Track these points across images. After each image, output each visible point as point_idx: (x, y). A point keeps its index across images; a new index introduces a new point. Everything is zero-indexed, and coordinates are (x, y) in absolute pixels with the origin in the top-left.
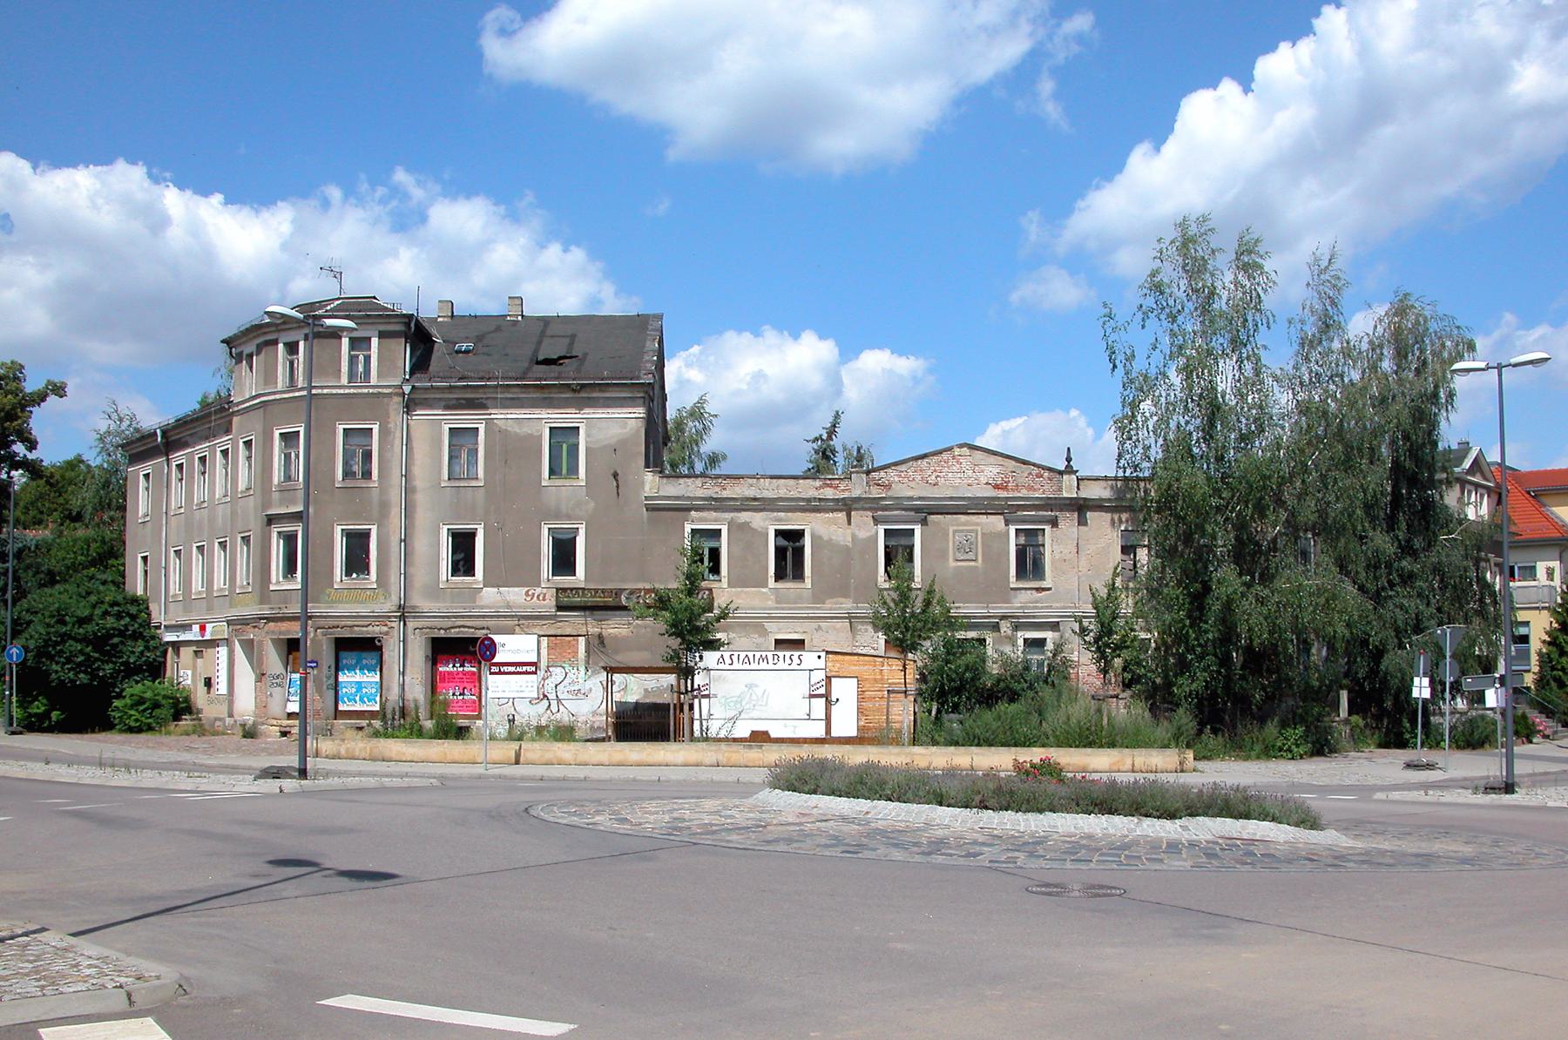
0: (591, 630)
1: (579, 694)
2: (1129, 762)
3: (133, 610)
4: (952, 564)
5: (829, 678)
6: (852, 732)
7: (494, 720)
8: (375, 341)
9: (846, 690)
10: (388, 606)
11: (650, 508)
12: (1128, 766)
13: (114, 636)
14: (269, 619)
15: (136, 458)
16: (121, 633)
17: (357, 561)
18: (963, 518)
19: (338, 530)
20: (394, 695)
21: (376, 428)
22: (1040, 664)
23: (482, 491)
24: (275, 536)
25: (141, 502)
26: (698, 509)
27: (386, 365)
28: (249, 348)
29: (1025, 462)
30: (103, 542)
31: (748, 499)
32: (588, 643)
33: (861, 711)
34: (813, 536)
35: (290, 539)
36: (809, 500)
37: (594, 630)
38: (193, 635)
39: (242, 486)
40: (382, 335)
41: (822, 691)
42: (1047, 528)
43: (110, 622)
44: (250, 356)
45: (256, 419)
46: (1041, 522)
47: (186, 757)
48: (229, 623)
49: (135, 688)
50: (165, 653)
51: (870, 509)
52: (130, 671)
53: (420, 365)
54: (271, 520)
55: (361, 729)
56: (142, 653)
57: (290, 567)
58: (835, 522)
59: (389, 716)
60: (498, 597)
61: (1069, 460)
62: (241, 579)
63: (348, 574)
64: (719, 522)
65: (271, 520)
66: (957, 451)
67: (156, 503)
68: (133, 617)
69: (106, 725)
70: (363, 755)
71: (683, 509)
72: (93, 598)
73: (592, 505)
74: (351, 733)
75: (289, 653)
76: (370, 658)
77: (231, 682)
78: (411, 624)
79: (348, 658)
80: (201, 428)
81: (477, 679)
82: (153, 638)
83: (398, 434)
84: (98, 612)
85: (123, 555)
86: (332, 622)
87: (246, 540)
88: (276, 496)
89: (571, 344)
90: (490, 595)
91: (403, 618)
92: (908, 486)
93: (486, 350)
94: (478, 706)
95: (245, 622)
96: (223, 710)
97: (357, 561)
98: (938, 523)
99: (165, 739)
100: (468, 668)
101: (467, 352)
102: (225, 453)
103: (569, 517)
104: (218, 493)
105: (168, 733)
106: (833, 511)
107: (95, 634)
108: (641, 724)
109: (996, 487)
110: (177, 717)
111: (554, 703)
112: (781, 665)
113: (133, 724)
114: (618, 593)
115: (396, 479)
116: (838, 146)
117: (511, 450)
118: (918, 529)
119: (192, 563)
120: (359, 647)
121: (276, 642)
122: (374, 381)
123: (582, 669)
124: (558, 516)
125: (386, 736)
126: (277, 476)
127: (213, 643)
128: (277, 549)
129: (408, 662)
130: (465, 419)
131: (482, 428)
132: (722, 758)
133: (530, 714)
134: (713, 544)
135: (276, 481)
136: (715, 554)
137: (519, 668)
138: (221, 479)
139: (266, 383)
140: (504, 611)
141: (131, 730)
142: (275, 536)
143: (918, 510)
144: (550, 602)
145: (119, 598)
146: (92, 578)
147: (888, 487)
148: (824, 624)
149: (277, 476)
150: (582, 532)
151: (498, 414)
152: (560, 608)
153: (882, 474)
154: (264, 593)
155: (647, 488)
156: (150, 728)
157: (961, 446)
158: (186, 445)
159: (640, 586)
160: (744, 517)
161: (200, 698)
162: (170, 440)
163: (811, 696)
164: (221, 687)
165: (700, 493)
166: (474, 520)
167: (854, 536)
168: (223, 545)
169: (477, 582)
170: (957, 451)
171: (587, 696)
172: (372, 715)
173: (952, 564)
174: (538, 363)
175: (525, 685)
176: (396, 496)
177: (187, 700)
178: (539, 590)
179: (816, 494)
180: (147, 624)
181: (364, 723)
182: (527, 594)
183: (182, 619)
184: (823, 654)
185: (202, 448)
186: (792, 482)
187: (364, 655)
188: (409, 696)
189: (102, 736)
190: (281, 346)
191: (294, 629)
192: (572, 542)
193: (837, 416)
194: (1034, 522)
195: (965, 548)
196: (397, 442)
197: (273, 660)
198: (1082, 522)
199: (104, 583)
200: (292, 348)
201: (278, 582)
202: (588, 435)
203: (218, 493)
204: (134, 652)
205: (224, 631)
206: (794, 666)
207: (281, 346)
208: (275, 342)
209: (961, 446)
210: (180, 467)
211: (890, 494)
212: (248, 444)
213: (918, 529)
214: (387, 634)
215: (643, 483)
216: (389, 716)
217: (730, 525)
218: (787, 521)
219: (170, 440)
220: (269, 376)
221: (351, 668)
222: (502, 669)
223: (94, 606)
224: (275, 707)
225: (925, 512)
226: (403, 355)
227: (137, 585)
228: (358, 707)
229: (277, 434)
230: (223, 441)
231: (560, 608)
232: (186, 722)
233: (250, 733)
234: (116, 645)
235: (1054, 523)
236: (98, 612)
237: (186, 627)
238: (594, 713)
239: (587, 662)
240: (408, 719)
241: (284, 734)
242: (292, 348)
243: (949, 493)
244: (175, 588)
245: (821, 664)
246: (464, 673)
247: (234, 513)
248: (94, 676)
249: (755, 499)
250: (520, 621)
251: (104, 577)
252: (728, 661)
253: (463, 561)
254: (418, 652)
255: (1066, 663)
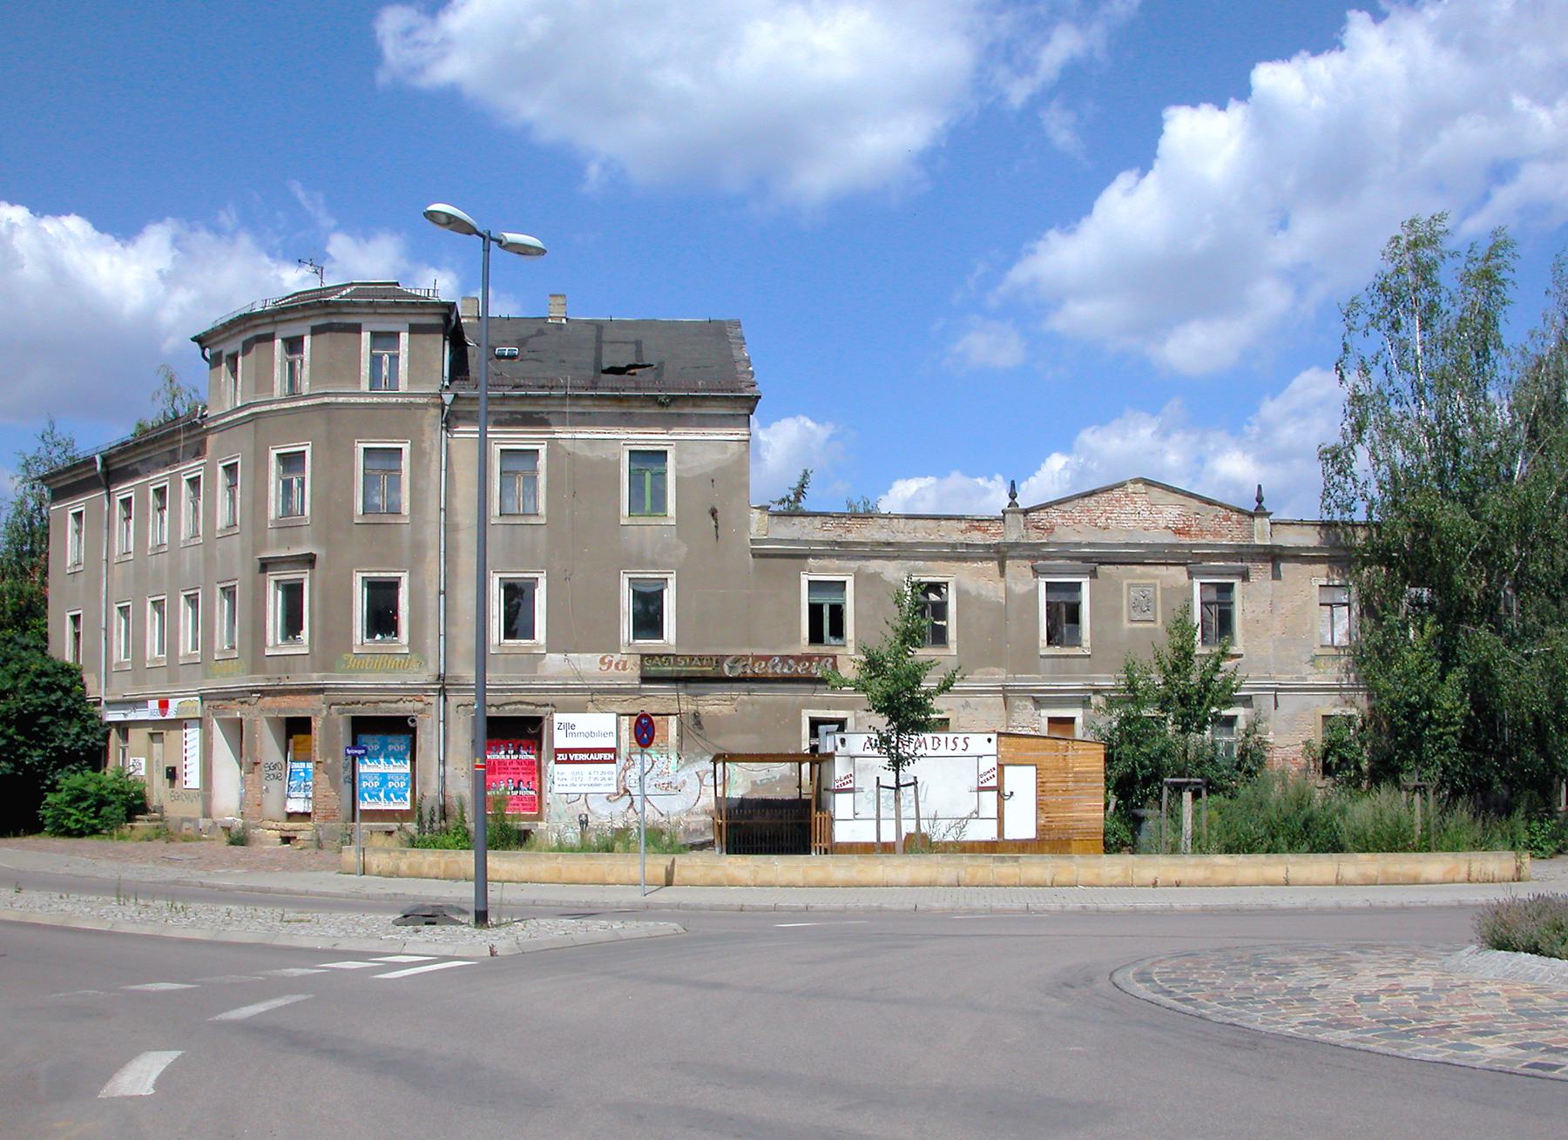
0: (684, 708)
1: (670, 788)
2: (1464, 869)
3: (66, 682)
4: (1126, 625)
5: (1001, 767)
6: (1029, 833)
7: (556, 823)
8: (404, 337)
9: (1021, 780)
10: (423, 676)
11: (757, 555)
12: (1463, 875)
13: (43, 714)
14: (264, 693)
15: (60, 494)
16: (52, 710)
17: (382, 619)
18: (1139, 569)
19: (358, 580)
20: (431, 791)
21: (406, 448)
22: (1229, 747)
23: (543, 531)
24: (271, 586)
25: (69, 548)
26: (816, 556)
27: (416, 366)
28: (235, 345)
29: (1210, 502)
30: (20, 596)
31: (879, 544)
32: (681, 723)
33: (1041, 806)
34: (959, 592)
35: (293, 593)
36: (954, 546)
37: (688, 706)
38: (151, 712)
39: (222, 520)
40: (414, 330)
41: (993, 783)
42: (1237, 582)
43: (36, 699)
44: (233, 358)
45: (244, 436)
46: (1230, 575)
47: (171, 873)
48: (203, 698)
49: (72, 780)
50: (107, 736)
51: (1028, 557)
52: (65, 759)
53: (459, 368)
54: (265, 565)
55: (390, 833)
56: (78, 735)
57: (292, 624)
58: (983, 573)
59: (427, 817)
60: (565, 666)
61: (1260, 500)
62: (221, 642)
63: (371, 635)
64: (842, 572)
65: (265, 565)
66: (1130, 488)
67: (93, 549)
68: (67, 691)
69: (34, 827)
70: (434, 872)
71: (797, 556)
72: (14, 667)
73: (684, 550)
74: (379, 840)
75: (289, 736)
76: (398, 743)
77: (200, 772)
78: (454, 700)
79: (371, 742)
80: (157, 453)
81: (536, 770)
82: (91, 717)
83: (435, 457)
84: (22, 684)
85: (44, 614)
86: (351, 697)
87: (229, 593)
88: (272, 535)
89: (639, 351)
90: (555, 663)
91: (443, 692)
92: (1073, 530)
93: (532, 355)
94: (536, 804)
95: (228, 696)
96: (196, 808)
97: (382, 619)
98: (1109, 576)
99: (128, 845)
100: (525, 756)
101: (512, 357)
102: (194, 483)
103: (655, 565)
104: (185, 532)
105: (122, 838)
106: (982, 559)
107: (19, 711)
108: (777, 827)
109: (1178, 532)
110: (130, 817)
111: (638, 800)
112: (942, 751)
113: (73, 826)
114: (720, 660)
115: (433, 514)
116: (816, 180)
117: (581, 479)
118: (1086, 583)
119: (143, 623)
120: (385, 729)
121: (270, 720)
122: (403, 387)
123: (674, 757)
124: (640, 563)
125: (425, 845)
126: (274, 509)
127: (180, 724)
128: (274, 604)
129: (450, 749)
130: (521, 438)
131: (543, 449)
132: (965, 876)
133: (608, 815)
134: (835, 600)
135: (272, 514)
136: (837, 612)
137: (593, 755)
138: (179, 517)
139: (258, 390)
140: (574, 683)
141: (69, 833)
142: (271, 586)
143: (1086, 559)
144: (632, 672)
145: (48, 667)
146: (11, 640)
147: (1050, 530)
148: (972, 700)
149: (274, 509)
150: (672, 583)
151: (563, 433)
152: (645, 679)
153: (1042, 514)
154: (257, 660)
155: (753, 529)
156: (95, 831)
157: (1136, 481)
158: (135, 474)
159: (747, 652)
160: (874, 566)
161: (158, 792)
162: (111, 470)
163: (980, 789)
164: (192, 778)
165: (819, 536)
166: (533, 567)
167: (1007, 590)
168: (192, 600)
169: (538, 646)
170: (1130, 488)
171: (685, 790)
172: (403, 815)
173: (1126, 625)
174: (605, 372)
175: (601, 778)
176: (433, 535)
177: (141, 795)
178: (617, 657)
179: (961, 538)
180: (82, 698)
181: (394, 826)
182: (602, 660)
183: (130, 694)
184: (994, 737)
185: (160, 477)
186: (931, 523)
187: (390, 739)
188: (452, 791)
189: (30, 840)
190: (278, 343)
191: (298, 707)
192: (659, 595)
193: (806, 475)
194: (1221, 575)
195: (1142, 606)
196: (434, 466)
197: (269, 746)
198: (1276, 576)
199: (26, 648)
200: (294, 345)
201: (276, 646)
202: (678, 462)
203: (185, 532)
204: (67, 735)
205: (195, 707)
206: (958, 752)
207: (278, 343)
208: (270, 338)
209: (1136, 481)
210: (126, 503)
211: (1052, 539)
212: (231, 470)
213: (1086, 583)
214: (422, 711)
215: (748, 524)
216: (427, 817)
217: (857, 575)
218: (927, 571)
219: (111, 470)
220: (263, 380)
221: (373, 756)
222: (568, 756)
223: (15, 677)
224: (272, 806)
225: (1095, 561)
226: (439, 353)
227: (64, 649)
228: (383, 805)
229: (273, 454)
230: (191, 468)
231: (645, 679)
232: (142, 824)
233: (239, 839)
234: (46, 726)
235: (1245, 576)
236: (22, 684)
237: (141, 703)
238: (689, 812)
239: (680, 747)
240: (451, 821)
241: (286, 840)
242: (294, 345)
243: (1123, 539)
244: (119, 654)
245: (992, 748)
246: (519, 762)
247: (209, 560)
248: (19, 764)
249: (889, 544)
250: (592, 696)
251: (25, 641)
252: (961, 745)
253: (517, 623)
254: (463, 735)
255: (1261, 743)
